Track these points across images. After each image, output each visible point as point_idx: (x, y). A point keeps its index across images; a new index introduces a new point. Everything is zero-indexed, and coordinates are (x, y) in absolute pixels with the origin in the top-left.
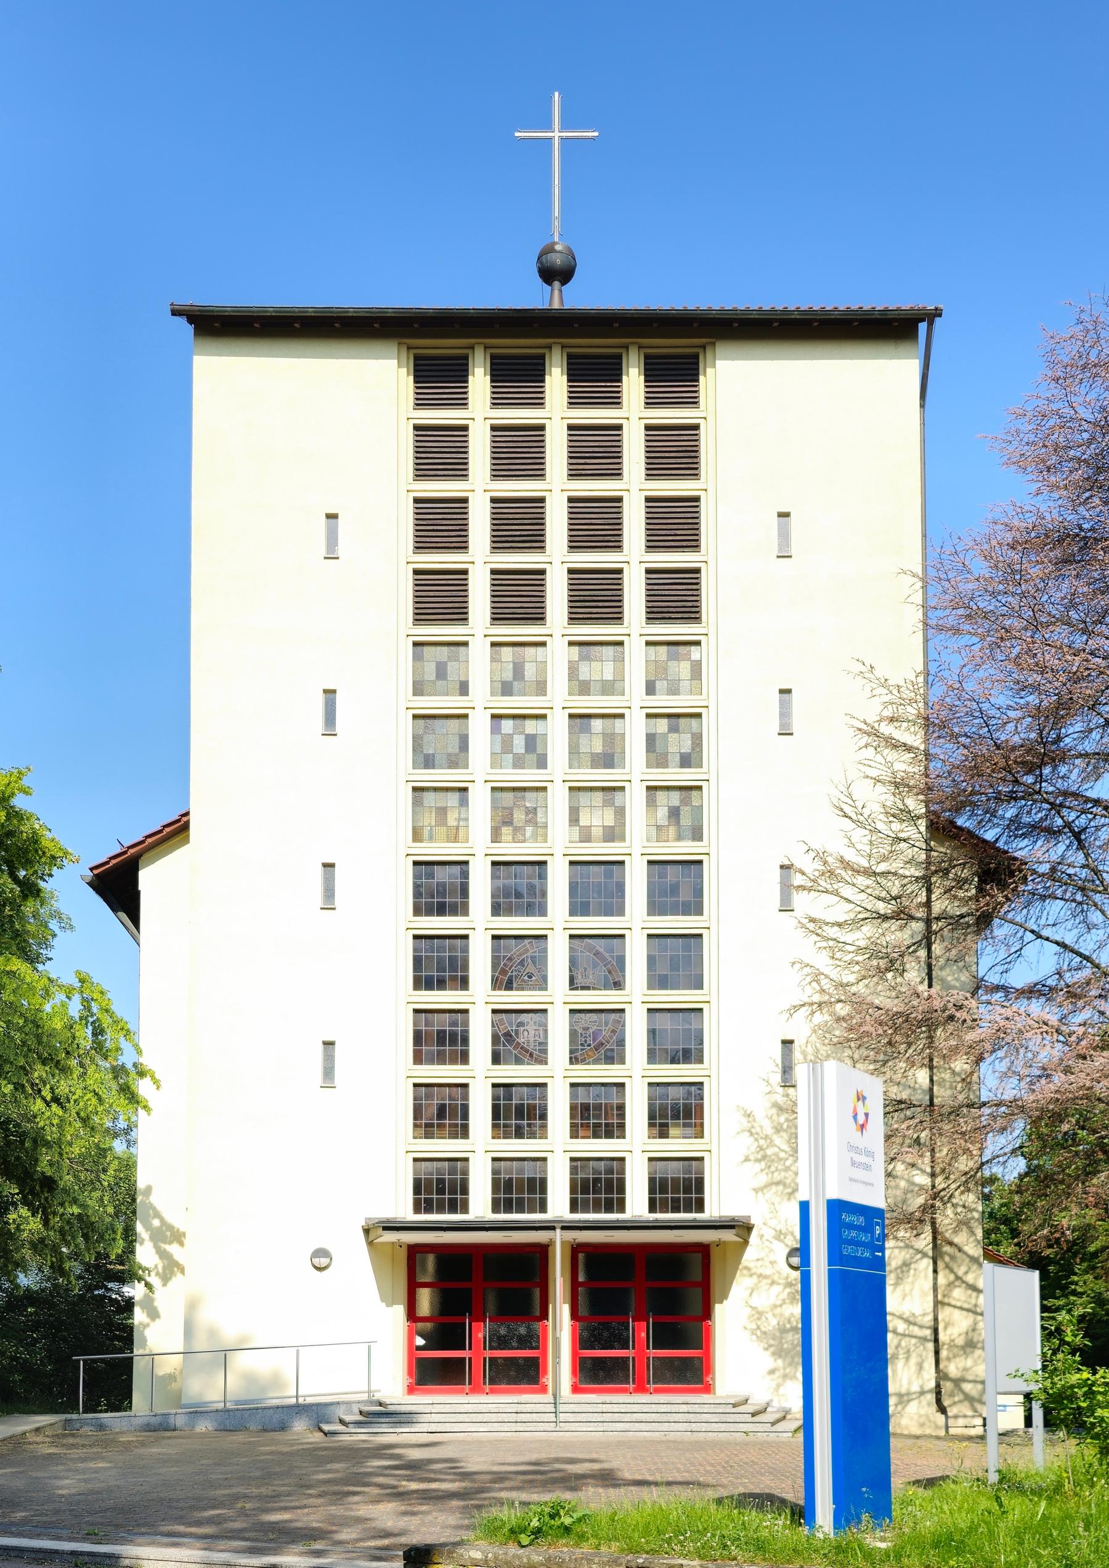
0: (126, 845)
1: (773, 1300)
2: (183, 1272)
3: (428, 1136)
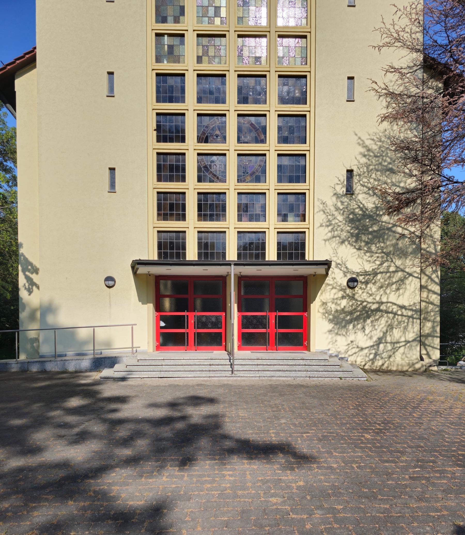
0: (6, 63)
1: (332, 296)
2: (38, 288)
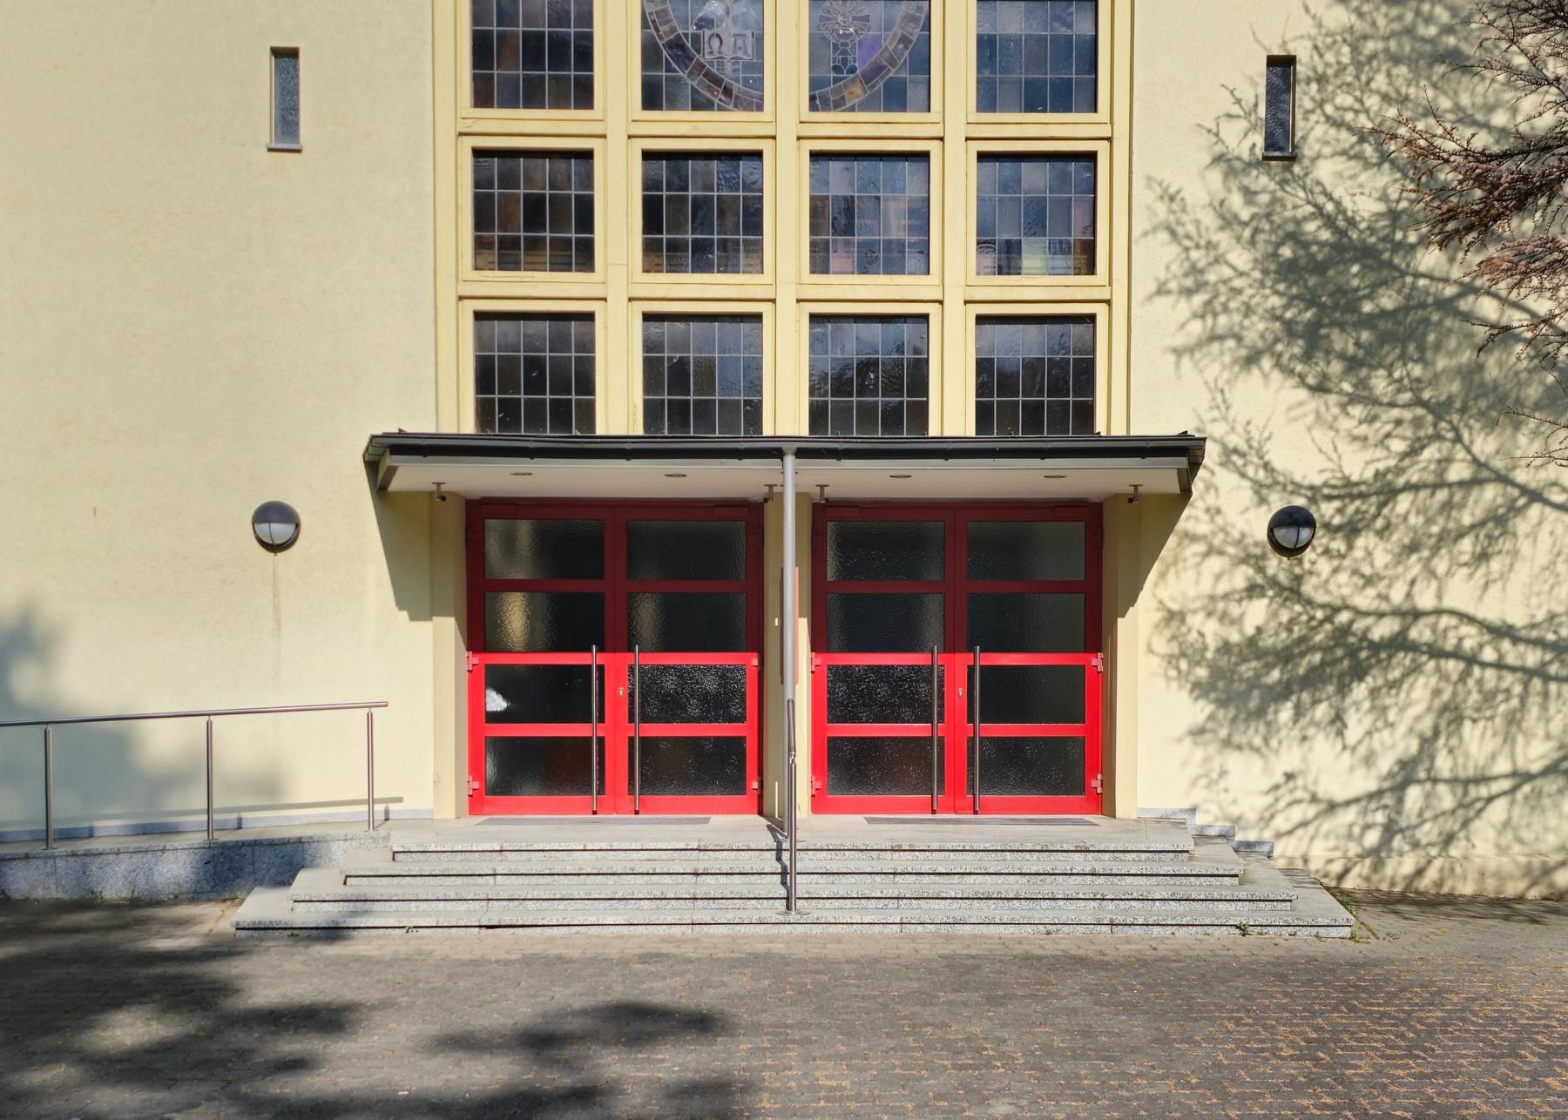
3: (508, 261)
